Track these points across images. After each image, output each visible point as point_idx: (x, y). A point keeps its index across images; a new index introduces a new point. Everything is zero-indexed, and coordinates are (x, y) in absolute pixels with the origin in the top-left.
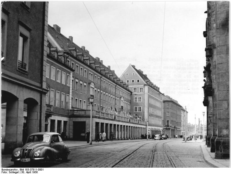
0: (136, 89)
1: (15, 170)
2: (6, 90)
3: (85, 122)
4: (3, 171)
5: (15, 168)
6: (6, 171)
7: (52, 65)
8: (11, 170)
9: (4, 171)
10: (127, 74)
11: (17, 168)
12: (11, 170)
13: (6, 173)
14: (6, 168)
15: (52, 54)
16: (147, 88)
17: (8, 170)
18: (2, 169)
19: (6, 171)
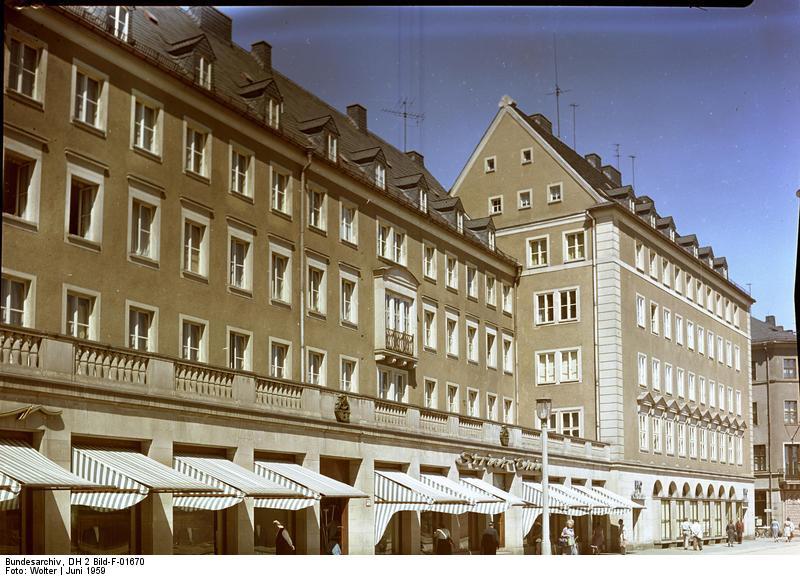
0: (543, 242)
1: (54, 563)
2: (68, 64)
3: (421, 514)
4: (10, 565)
5: (52, 557)
6: (19, 567)
7: (245, 113)
8: (39, 563)
9: (14, 567)
10: (491, 164)
11: (58, 557)
12: (39, 563)
13: (21, 571)
14: (20, 557)
15: (89, 14)
16: (607, 233)
17: (28, 562)
18: (8, 561)
19: (19, 567)
